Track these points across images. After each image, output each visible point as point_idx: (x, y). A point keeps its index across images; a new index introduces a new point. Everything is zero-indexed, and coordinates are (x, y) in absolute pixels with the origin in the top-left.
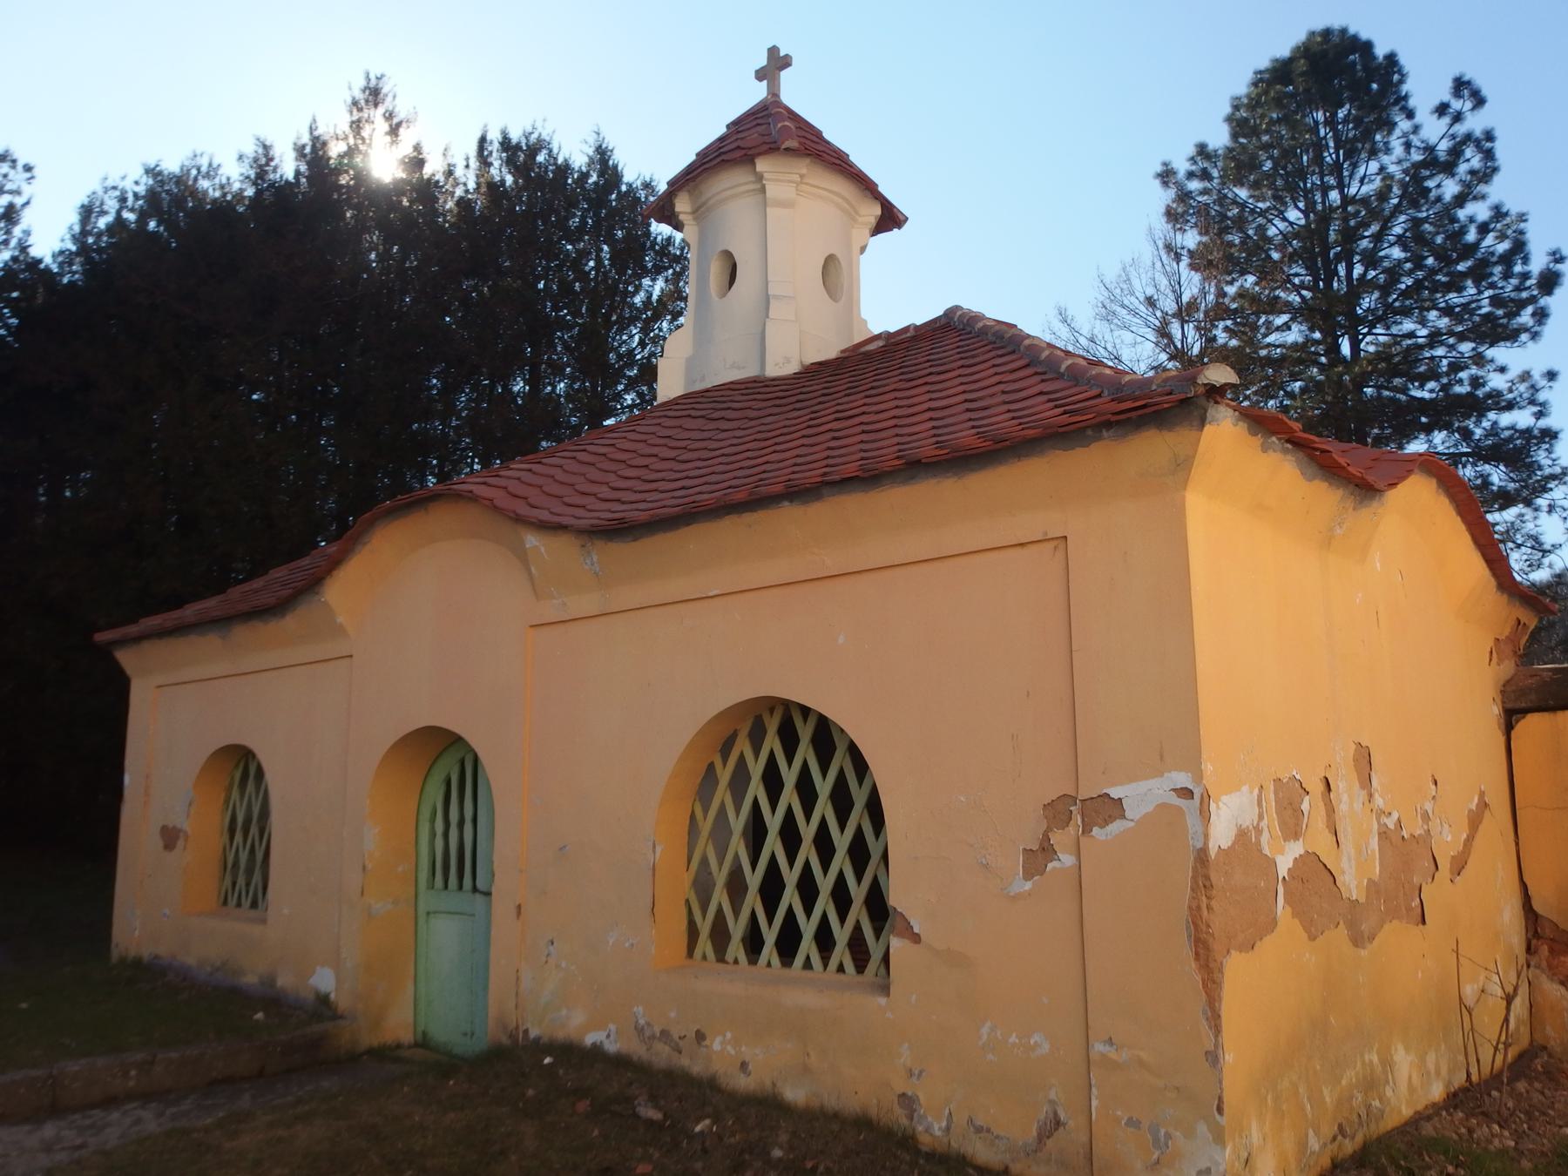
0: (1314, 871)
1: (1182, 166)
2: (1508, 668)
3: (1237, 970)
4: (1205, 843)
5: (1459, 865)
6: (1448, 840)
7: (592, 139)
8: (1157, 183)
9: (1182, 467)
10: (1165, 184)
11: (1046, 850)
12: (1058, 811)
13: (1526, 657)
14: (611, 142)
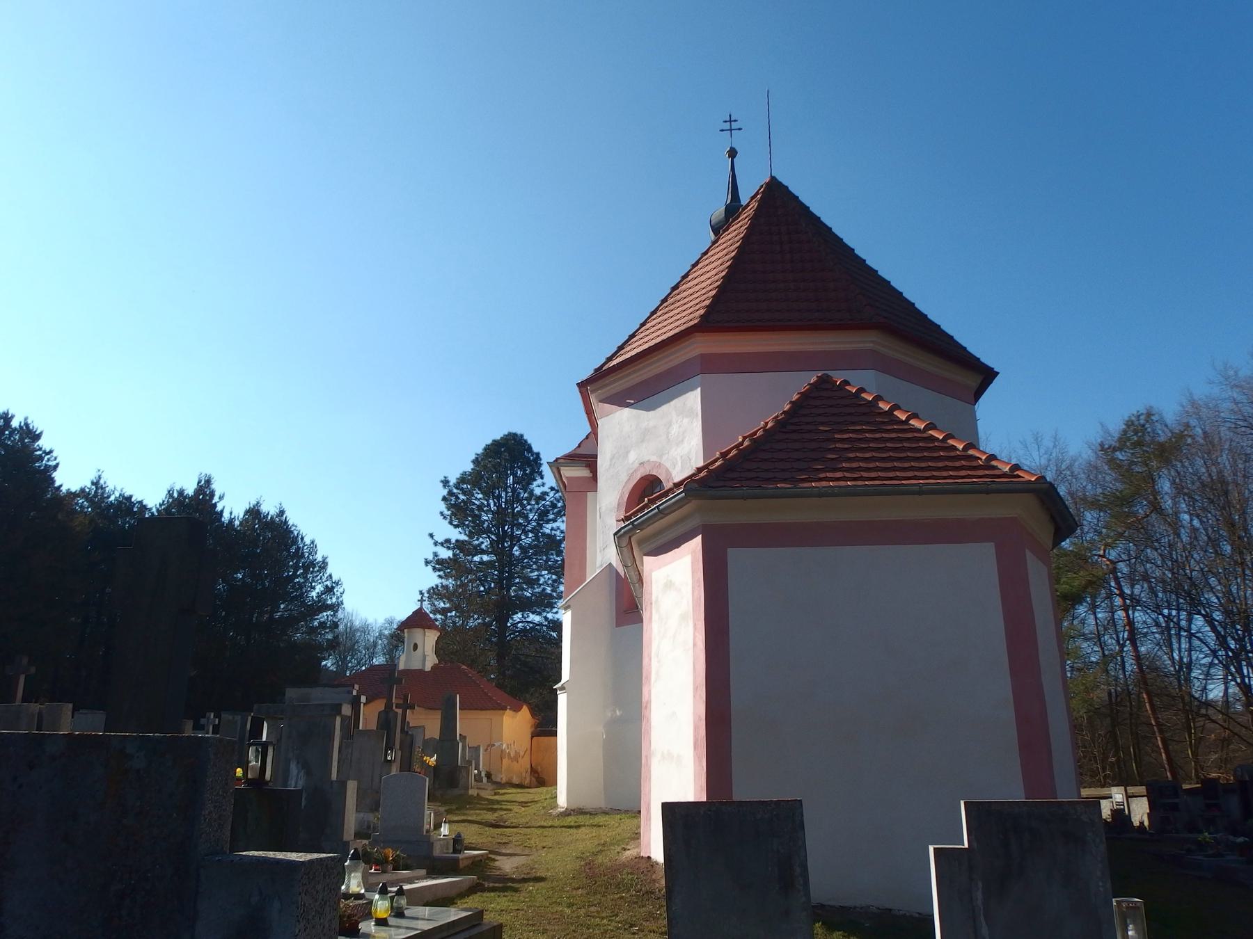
0: (509, 754)
1: (453, 481)
2: (533, 729)
3: (504, 760)
4: (1022, 470)
5: (523, 757)
6: (522, 753)
7: (278, 507)
8: (441, 484)
9: (504, 714)
10: (444, 486)
11: (487, 749)
12: (489, 746)
13: (535, 728)
14: (285, 507)
